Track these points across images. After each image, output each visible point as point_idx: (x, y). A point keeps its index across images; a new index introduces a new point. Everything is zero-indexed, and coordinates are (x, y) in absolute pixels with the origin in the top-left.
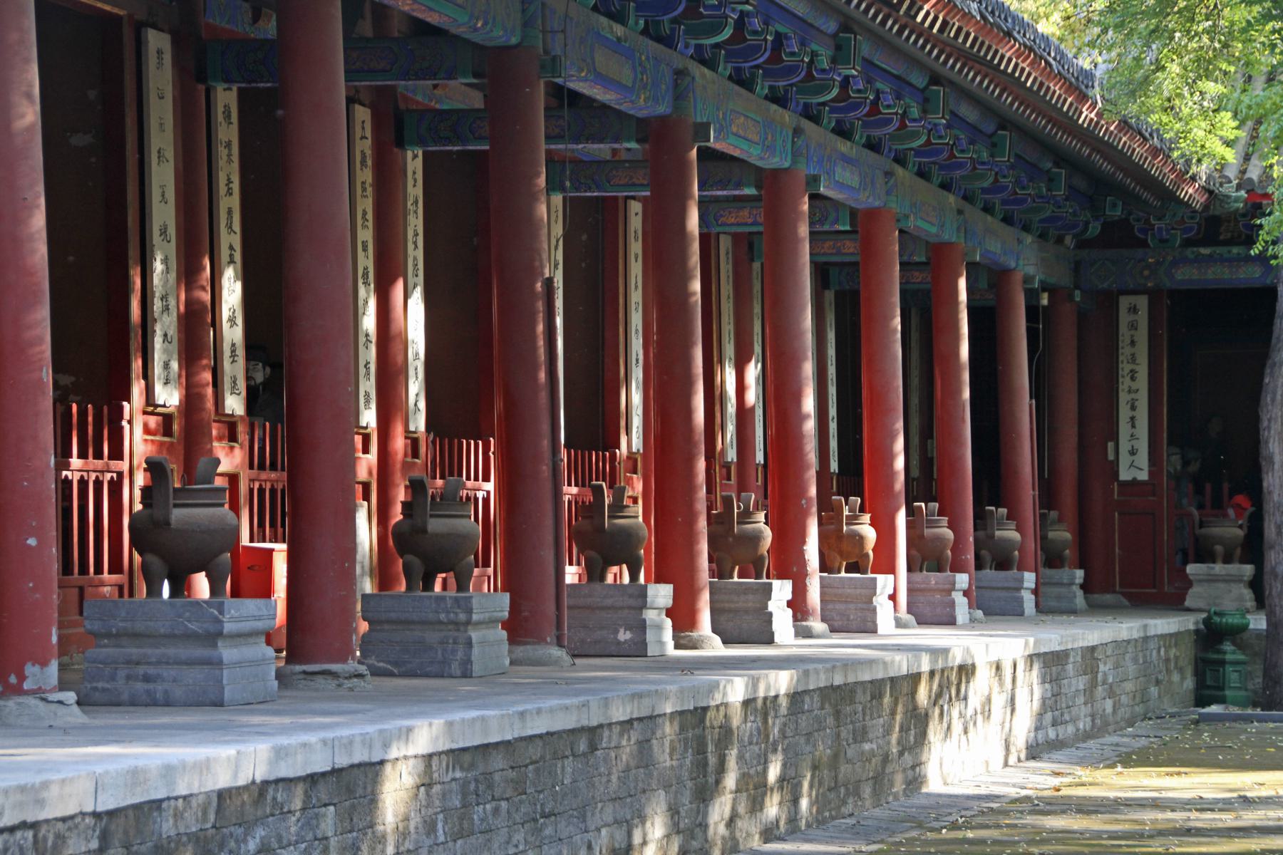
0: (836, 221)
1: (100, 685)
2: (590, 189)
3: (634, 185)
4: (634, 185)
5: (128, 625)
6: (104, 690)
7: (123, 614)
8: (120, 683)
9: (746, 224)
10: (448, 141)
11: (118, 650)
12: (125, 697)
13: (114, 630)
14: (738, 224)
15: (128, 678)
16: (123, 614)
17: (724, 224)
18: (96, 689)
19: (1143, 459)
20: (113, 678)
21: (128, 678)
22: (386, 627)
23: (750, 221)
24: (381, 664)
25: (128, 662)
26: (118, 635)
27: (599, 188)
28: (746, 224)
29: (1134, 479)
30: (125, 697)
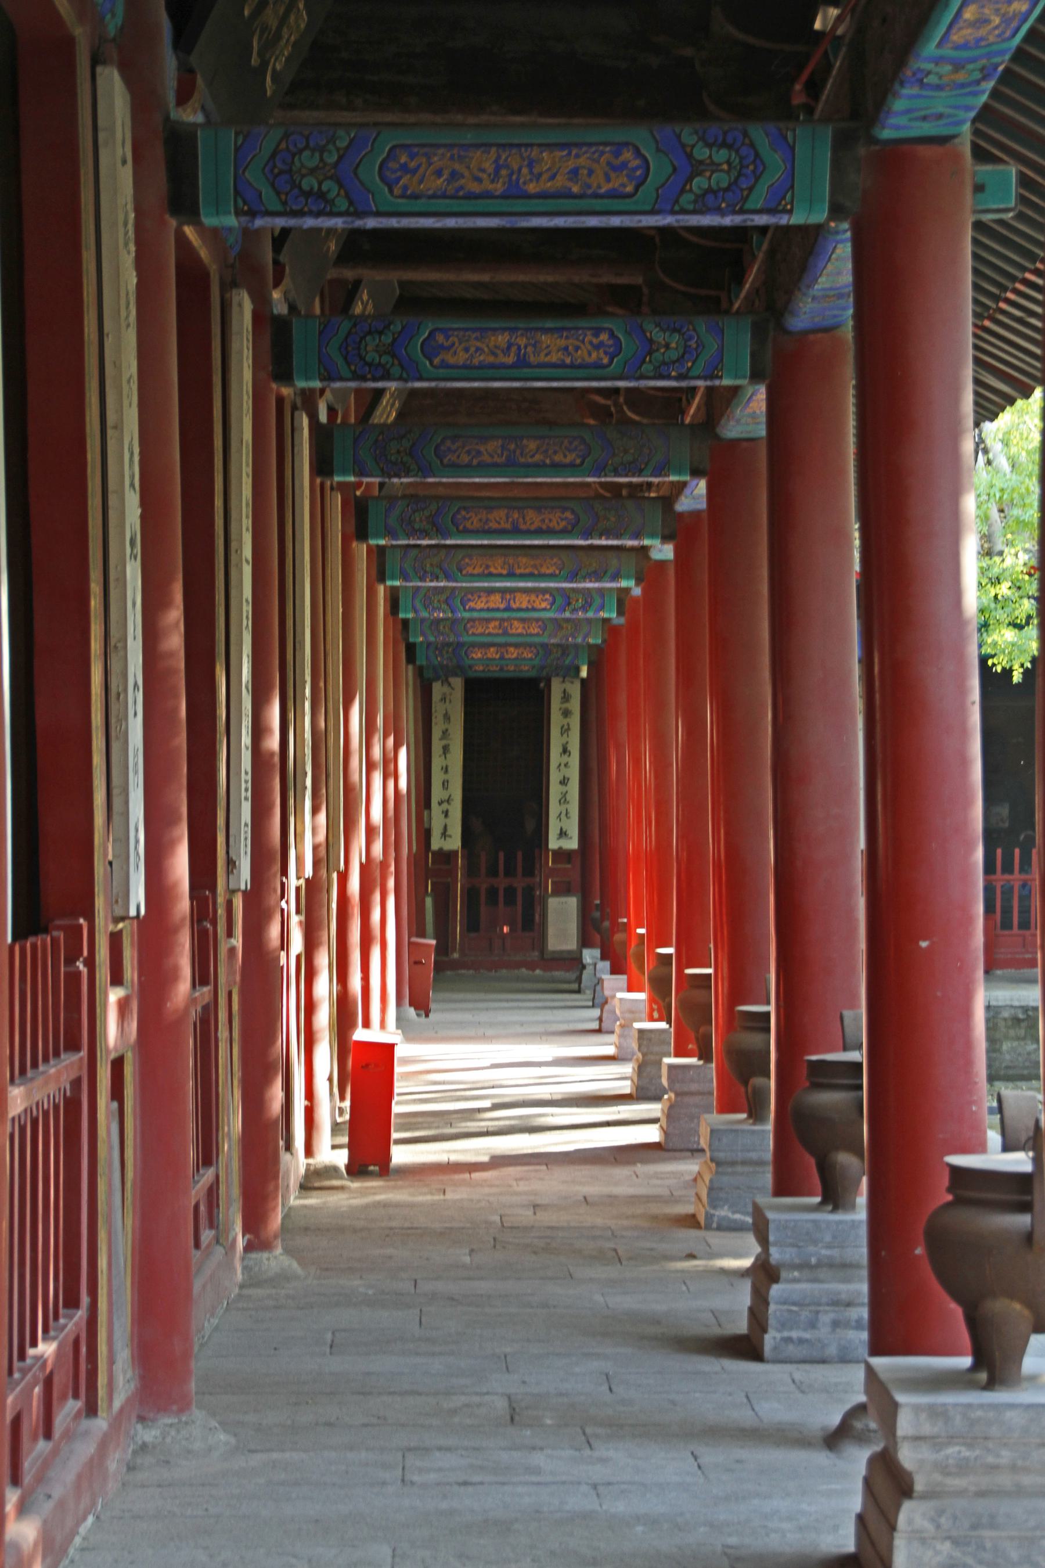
0: (602, 607)
1: (794, 1334)
2: (437, 579)
3: (491, 575)
4: (491, 575)
5: (835, 1253)
6: (801, 1341)
7: (828, 1238)
8: (823, 1331)
9: (498, 610)
10: (426, 534)
11: (816, 1286)
12: (832, 1350)
13: (813, 1260)
14: (488, 610)
15: (836, 1324)
16: (828, 1238)
17: (472, 610)
18: (789, 1340)
19: (574, 831)
20: (812, 1325)
21: (836, 1324)
22: (739, 1169)
23: (502, 606)
24: (737, 1216)
25: (835, 1303)
26: (819, 1265)
27: (448, 577)
28: (498, 610)
29: (560, 848)
30: (832, 1350)
